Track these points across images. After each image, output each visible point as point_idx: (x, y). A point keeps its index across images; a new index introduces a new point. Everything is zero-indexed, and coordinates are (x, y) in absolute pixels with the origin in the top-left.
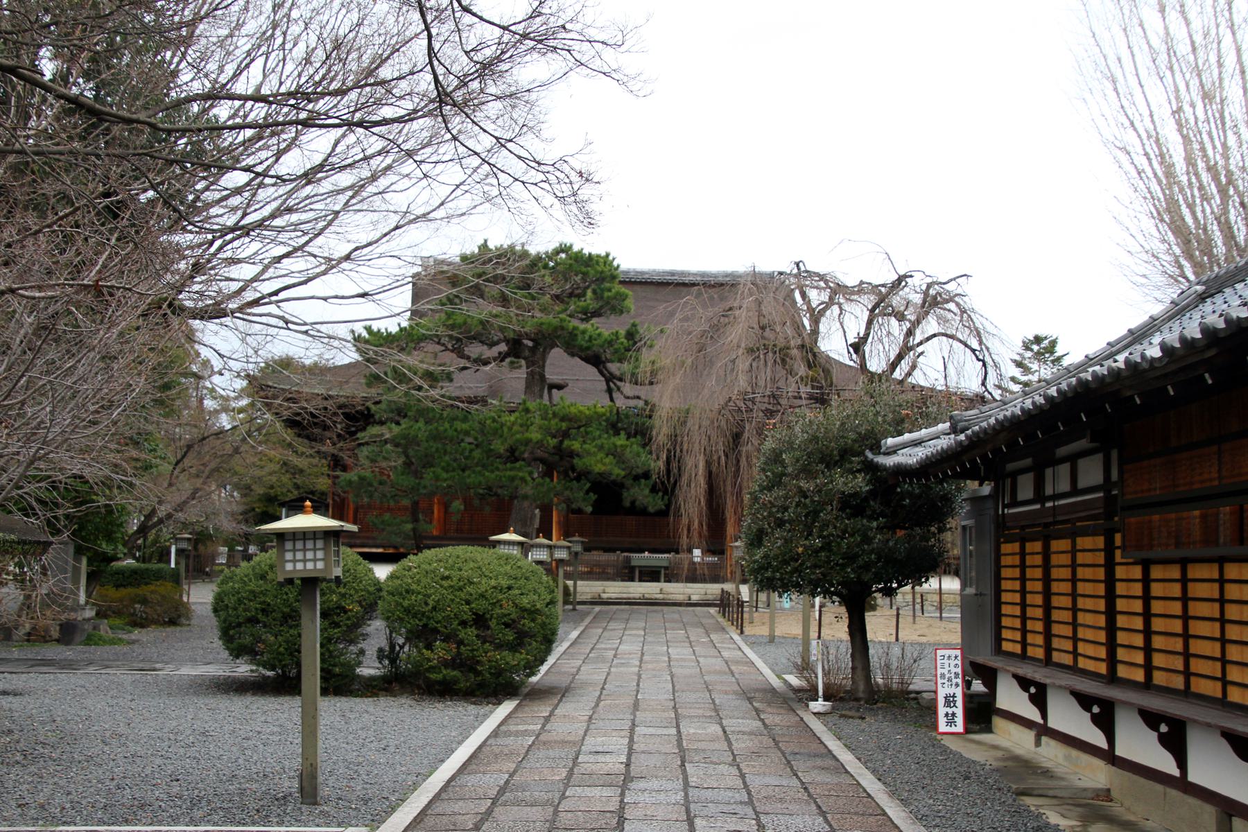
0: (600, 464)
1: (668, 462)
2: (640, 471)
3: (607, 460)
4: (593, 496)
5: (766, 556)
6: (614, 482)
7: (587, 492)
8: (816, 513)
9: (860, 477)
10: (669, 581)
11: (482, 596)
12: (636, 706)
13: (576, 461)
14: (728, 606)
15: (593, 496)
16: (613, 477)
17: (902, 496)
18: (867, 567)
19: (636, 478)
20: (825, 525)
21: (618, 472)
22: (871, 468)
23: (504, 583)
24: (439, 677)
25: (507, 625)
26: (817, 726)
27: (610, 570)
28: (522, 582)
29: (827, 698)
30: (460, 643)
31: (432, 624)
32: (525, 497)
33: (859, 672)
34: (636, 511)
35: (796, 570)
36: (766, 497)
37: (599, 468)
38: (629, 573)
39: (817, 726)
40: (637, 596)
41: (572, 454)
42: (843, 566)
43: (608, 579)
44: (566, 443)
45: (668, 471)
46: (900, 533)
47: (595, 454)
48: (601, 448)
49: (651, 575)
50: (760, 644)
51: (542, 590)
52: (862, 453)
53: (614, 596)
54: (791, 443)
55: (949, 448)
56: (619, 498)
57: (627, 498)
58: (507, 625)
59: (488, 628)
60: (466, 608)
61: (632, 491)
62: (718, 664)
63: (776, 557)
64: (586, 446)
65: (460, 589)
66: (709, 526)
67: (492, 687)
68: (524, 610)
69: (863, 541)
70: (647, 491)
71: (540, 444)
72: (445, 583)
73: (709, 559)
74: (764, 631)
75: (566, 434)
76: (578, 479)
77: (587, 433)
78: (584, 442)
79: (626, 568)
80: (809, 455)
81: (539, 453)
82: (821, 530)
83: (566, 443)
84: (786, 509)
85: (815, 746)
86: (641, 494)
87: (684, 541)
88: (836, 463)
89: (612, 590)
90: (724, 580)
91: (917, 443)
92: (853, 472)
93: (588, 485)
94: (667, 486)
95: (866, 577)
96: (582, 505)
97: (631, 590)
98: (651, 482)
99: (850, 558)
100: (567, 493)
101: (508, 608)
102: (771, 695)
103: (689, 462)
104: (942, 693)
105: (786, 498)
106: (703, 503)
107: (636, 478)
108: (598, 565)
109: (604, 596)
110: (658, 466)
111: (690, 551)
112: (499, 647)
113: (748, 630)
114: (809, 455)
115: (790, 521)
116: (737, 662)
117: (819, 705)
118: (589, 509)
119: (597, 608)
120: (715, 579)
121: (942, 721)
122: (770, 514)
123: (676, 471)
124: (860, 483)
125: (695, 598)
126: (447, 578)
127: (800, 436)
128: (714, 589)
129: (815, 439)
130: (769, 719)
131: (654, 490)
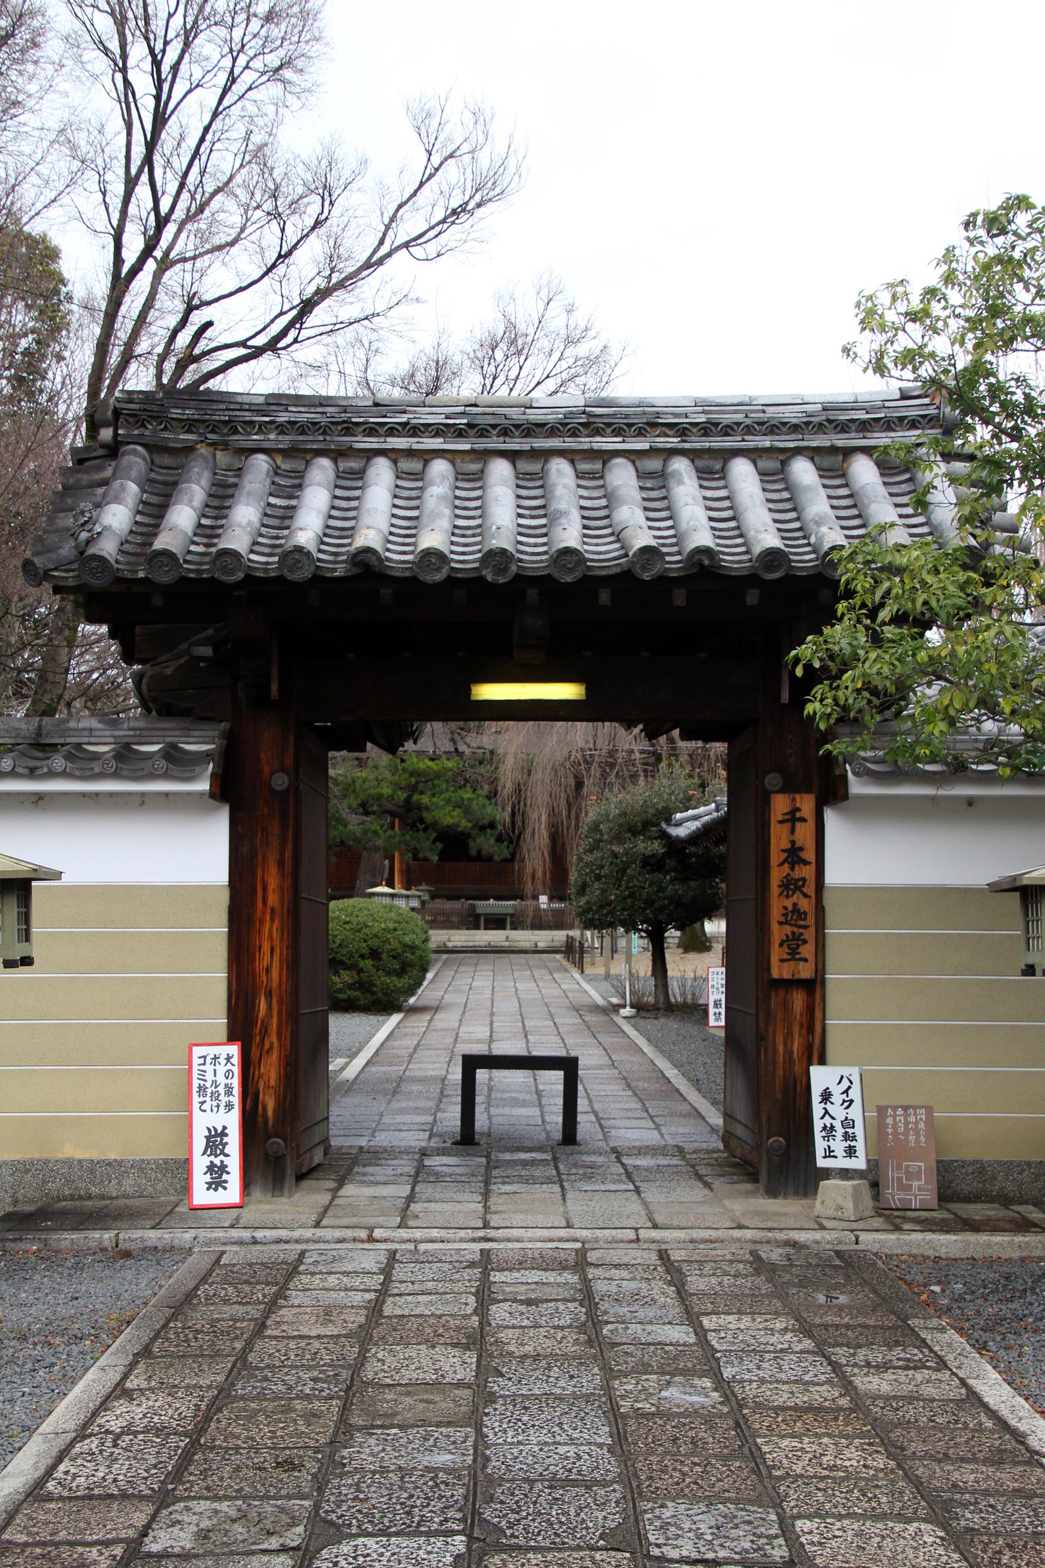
0: (449, 817)
1: (513, 814)
2: (486, 822)
3: (455, 813)
4: (439, 846)
5: (588, 903)
6: (462, 833)
7: (434, 842)
8: (624, 870)
9: (656, 843)
10: (515, 929)
11: (376, 936)
12: (492, 1014)
13: (425, 814)
14: (574, 952)
15: (439, 846)
16: (460, 829)
17: (691, 855)
18: (661, 909)
19: (482, 828)
20: (631, 879)
21: (465, 824)
22: (664, 836)
23: (391, 925)
24: (345, 996)
25: (394, 957)
26: (627, 1028)
27: (454, 919)
28: (404, 925)
29: (632, 1007)
30: (360, 971)
31: (339, 957)
32: (377, 849)
33: (660, 988)
34: (481, 857)
35: (609, 913)
36: (588, 858)
37: (448, 821)
38: (474, 921)
39: (627, 1028)
40: (483, 944)
41: (420, 807)
42: (644, 909)
43: (453, 928)
44: (416, 797)
45: (513, 823)
46: (693, 884)
47: (442, 808)
48: (448, 801)
49: (497, 922)
50: (597, 980)
51: (418, 931)
52: (658, 825)
53: (459, 944)
54: (607, 815)
55: (698, 829)
56: (466, 848)
57: (473, 847)
58: (394, 957)
59: (380, 959)
60: (364, 945)
61: (478, 841)
62: (558, 992)
63: (595, 903)
64: (434, 800)
65: (359, 931)
66: (551, 872)
67: (384, 1004)
68: (406, 946)
69: (658, 891)
70: (492, 841)
71: (391, 797)
72: (347, 927)
73: (556, 905)
74: (601, 971)
75: (414, 789)
76: (425, 830)
77: (434, 786)
78: (433, 795)
79: (470, 916)
80: (620, 826)
81: (388, 806)
82: (628, 882)
83: (416, 797)
84: (602, 867)
85: (615, 1029)
86: (486, 843)
87: (529, 888)
88: (640, 833)
89: (457, 938)
90: (571, 927)
91: (695, 818)
92: (651, 838)
93: (434, 835)
94: (513, 836)
95: (662, 917)
96: (429, 855)
97: (477, 938)
98: (496, 833)
99: (649, 903)
100: (414, 842)
101: (394, 944)
102: (596, 1009)
103: (533, 816)
104: (712, 999)
105: (602, 858)
106: (546, 854)
107: (482, 828)
108: (442, 913)
109: (450, 944)
110: (503, 816)
111: (536, 898)
112: (388, 974)
113: (588, 970)
114: (620, 826)
115: (605, 876)
116: (573, 991)
117: (627, 1011)
118: (436, 858)
119: (445, 956)
120: (559, 926)
121: (712, 1018)
122: (592, 871)
123: (520, 823)
124: (656, 847)
125: (541, 945)
126: (348, 923)
127: (614, 812)
128: (559, 936)
129: (623, 814)
130: (587, 1018)
131: (499, 839)
